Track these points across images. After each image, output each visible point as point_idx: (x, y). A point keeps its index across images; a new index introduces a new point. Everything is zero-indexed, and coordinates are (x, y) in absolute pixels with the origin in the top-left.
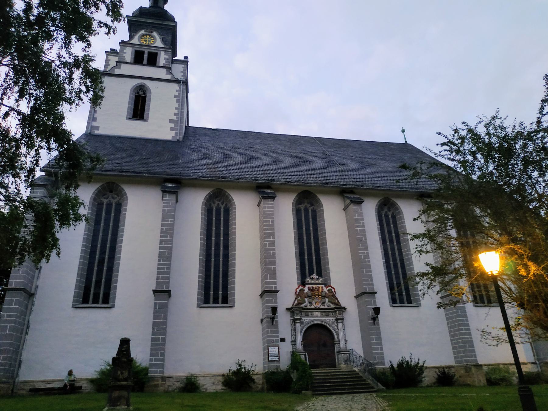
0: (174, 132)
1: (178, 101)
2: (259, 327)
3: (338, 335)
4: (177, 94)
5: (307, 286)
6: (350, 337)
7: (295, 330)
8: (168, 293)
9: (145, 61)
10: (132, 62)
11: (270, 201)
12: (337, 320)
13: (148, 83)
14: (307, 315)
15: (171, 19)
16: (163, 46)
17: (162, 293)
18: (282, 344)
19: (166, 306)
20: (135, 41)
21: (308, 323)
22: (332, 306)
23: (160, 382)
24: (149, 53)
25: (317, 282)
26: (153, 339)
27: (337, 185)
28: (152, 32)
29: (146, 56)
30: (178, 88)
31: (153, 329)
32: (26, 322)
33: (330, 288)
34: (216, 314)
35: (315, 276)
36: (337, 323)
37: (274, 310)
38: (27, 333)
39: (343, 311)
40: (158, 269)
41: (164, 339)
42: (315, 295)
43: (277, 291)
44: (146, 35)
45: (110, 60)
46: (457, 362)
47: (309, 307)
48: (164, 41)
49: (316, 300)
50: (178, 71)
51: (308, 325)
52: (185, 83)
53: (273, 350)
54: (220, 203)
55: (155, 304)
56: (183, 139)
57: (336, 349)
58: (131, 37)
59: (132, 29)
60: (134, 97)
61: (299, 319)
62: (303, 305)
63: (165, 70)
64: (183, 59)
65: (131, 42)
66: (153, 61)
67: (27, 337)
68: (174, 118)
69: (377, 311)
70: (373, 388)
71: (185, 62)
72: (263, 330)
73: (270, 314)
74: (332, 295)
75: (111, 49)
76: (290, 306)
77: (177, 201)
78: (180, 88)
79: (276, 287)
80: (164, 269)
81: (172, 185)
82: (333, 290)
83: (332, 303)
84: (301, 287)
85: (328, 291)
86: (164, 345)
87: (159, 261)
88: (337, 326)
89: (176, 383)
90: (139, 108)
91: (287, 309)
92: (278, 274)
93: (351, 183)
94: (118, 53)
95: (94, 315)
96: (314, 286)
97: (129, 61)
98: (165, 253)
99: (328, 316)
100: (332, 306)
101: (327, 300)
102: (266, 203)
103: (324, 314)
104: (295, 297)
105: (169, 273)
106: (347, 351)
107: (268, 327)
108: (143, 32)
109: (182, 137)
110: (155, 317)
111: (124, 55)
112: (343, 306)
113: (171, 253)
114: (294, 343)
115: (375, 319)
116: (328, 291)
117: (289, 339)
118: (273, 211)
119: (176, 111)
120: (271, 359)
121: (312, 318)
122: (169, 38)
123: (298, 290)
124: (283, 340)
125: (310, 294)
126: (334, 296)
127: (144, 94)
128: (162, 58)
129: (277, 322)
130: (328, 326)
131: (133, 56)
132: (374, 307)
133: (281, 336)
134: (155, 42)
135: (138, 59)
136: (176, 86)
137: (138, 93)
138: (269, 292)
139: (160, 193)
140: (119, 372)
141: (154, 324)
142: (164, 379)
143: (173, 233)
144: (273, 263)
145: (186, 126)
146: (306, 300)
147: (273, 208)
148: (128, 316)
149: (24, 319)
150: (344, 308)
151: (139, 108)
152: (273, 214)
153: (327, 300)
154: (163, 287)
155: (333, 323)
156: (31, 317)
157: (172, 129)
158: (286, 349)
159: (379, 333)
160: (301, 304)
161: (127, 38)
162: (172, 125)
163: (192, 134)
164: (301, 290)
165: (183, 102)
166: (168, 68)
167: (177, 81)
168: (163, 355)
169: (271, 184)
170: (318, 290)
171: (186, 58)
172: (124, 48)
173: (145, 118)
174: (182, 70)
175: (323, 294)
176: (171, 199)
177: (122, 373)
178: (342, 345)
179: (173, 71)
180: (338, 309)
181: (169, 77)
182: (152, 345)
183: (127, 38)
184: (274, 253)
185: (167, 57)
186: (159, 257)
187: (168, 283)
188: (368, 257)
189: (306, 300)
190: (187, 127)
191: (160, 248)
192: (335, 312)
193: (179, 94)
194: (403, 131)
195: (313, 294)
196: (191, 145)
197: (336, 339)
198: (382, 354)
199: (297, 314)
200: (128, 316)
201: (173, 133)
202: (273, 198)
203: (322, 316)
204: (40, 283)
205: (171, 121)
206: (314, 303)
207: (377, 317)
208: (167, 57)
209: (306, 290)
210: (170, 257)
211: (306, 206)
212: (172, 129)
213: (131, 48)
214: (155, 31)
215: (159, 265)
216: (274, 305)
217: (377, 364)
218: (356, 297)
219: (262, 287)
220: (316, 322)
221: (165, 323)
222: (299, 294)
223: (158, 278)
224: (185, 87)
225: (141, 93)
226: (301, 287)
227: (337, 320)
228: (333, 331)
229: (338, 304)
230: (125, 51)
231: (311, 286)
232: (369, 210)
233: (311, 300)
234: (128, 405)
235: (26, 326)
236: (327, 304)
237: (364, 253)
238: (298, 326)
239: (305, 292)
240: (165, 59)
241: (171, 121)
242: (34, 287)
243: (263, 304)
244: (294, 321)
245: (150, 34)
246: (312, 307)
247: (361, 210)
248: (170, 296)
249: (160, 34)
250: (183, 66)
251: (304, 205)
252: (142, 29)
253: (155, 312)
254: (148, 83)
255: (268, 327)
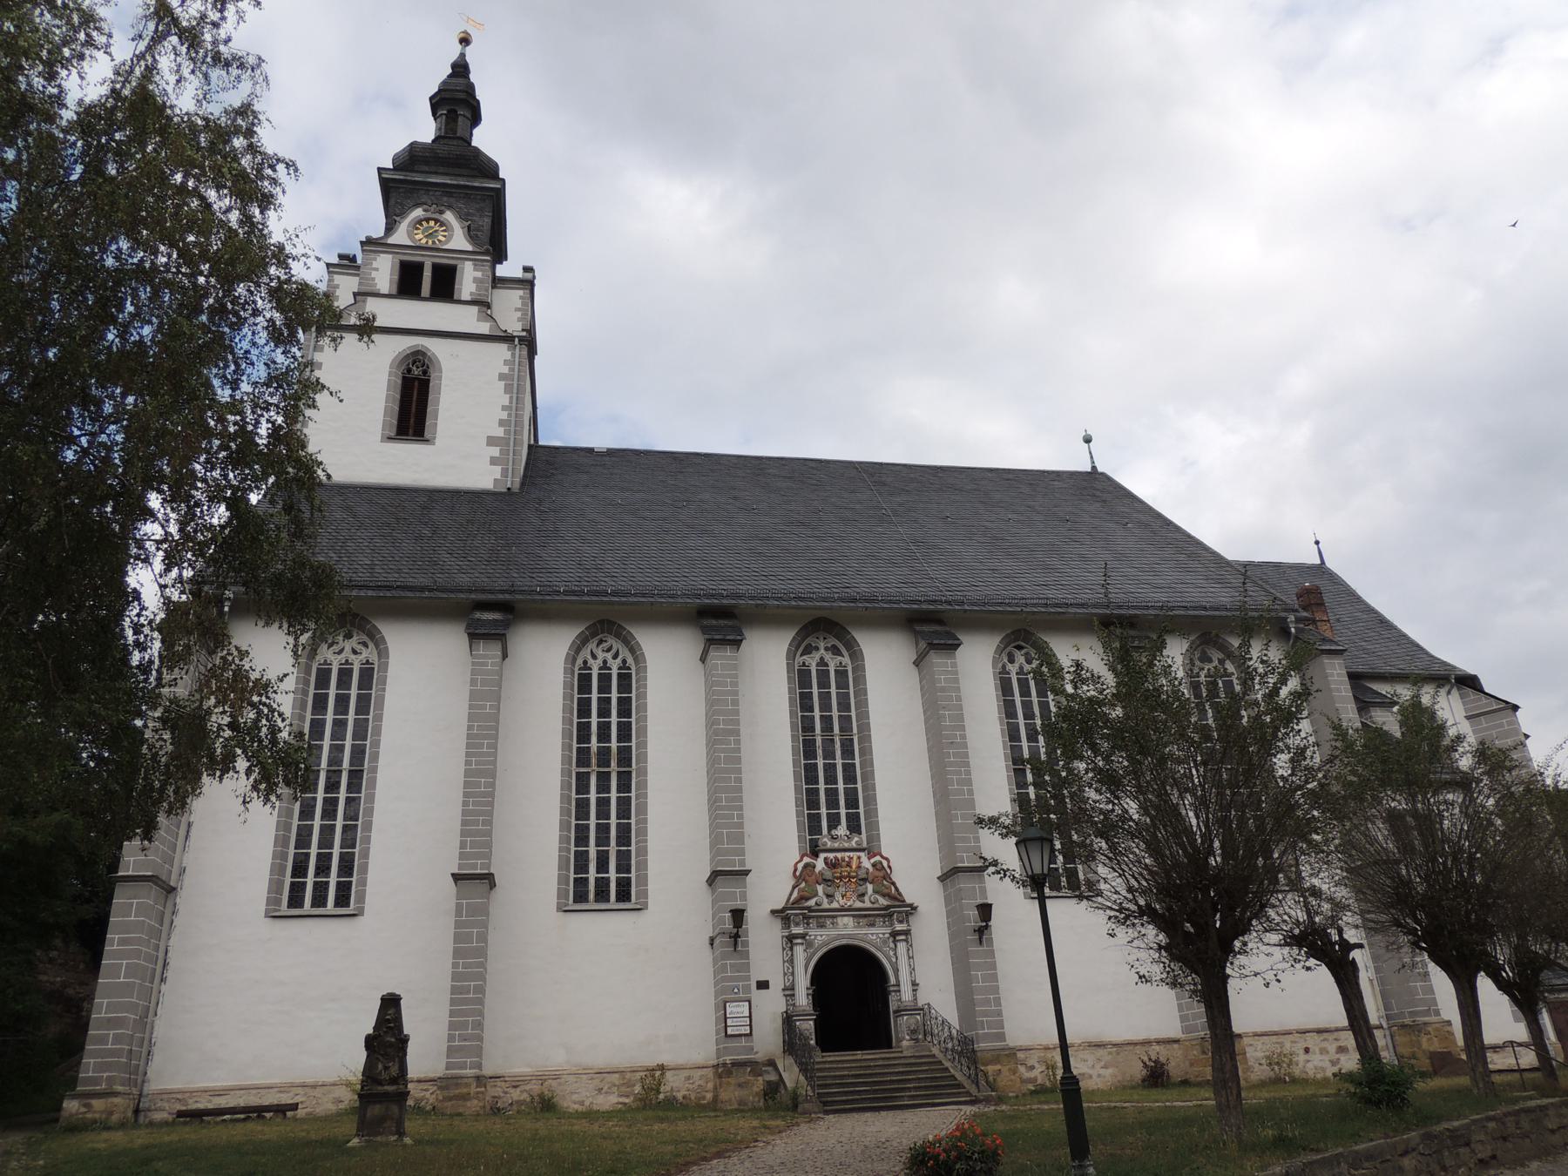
0: (498, 469)
1: (508, 389)
2: (706, 955)
3: (896, 971)
4: (506, 370)
5: (822, 856)
6: (925, 977)
7: (791, 961)
8: (488, 879)
9: (426, 288)
10: (394, 292)
11: (728, 652)
12: (894, 934)
13: (434, 346)
14: (822, 926)
15: (488, 169)
16: (469, 248)
17: (475, 881)
18: (756, 995)
19: (484, 911)
20: (400, 237)
21: (825, 944)
22: (883, 902)
23: (473, 1089)
24: (437, 268)
25: (846, 845)
26: (454, 990)
27: (898, 602)
28: (442, 212)
29: (427, 274)
30: (508, 355)
31: (455, 965)
32: (161, 955)
33: (878, 858)
34: (602, 928)
35: (842, 830)
36: (895, 942)
37: (738, 915)
38: (163, 980)
39: (908, 914)
40: (464, 823)
41: (481, 990)
42: (840, 878)
43: (746, 873)
44: (428, 220)
45: (337, 286)
46: (1186, 1030)
47: (826, 905)
48: (471, 234)
49: (842, 889)
50: (507, 305)
51: (825, 950)
52: (528, 342)
53: (737, 1010)
54: (609, 656)
55: (459, 908)
56: (523, 484)
57: (893, 1006)
58: (390, 228)
59: (392, 202)
60: (399, 382)
61: (803, 936)
62: (812, 903)
63: (475, 309)
64: (519, 274)
65: (390, 241)
66: (444, 287)
67: (163, 987)
68: (500, 432)
69: (985, 910)
70: (968, 1093)
71: (527, 283)
72: (715, 961)
73: (729, 925)
74: (882, 876)
75: (341, 257)
76: (780, 906)
77: (505, 656)
78: (513, 355)
79: (742, 862)
80: (476, 823)
81: (492, 616)
82: (885, 863)
83: (884, 895)
84: (807, 860)
85: (874, 865)
86: (481, 1002)
87: (465, 804)
88: (895, 949)
89: (511, 1090)
90: (412, 411)
91: (773, 912)
92: (747, 829)
93: (933, 595)
94: (358, 268)
95: (316, 936)
96: (839, 855)
97: (385, 289)
98: (478, 785)
99: (872, 925)
100: (883, 902)
101: (870, 887)
102: (719, 656)
103: (863, 921)
104: (792, 882)
105: (489, 833)
106: (915, 1009)
107: (724, 956)
108: (418, 213)
109: (518, 480)
110: (457, 938)
111: (374, 274)
112: (908, 901)
113: (493, 785)
114: (789, 991)
115: (982, 931)
116: (874, 865)
117: (777, 983)
118: (736, 676)
119: (504, 415)
120: (730, 1031)
121: (834, 932)
122: (486, 222)
123: (800, 866)
124: (763, 985)
125: (828, 874)
126: (887, 877)
127: (425, 372)
128: (469, 280)
129: (746, 944)
130: (873, 950)
131: (396, 277)
132: (980, 901)
133: (757, 975)
134: (449, 238)
135: (408, 283)
136: (501, 351)
137: (409, 371)
138: (726, 875)
139: (464, 640)
140: (380, 1066)
141: (457, 953)
142: (479, 1079)
143: (496, 737)
144: (736, 802)
145: (530, 446)
146: (820, 889)
147: (735, 667)
148: (392, 940)
149: (157, 948)
150: (911, 905)
151: (412, 411)
152: (735, 684)
153: (870, 887)
154: (474, 866)
155: (885, 942)
156: (171, 943)
157: (494, 461)
158: (771, 1006)
159: (993, 966)
160: (807, 899)
161: (378, 231)
162: (495, 451)
163: (547, 468)
164: (806, 866)
165: (520, 390)
166: (482, 304)
167: (507, 338)
168: (479, 1025)
169: (734, 606)
170: (849, 865)
171: (527, 269)
172: (372, 256)
173: (427, 435)
174: (519, 304)
175: (862, 874)
176: (490, 651)
177: (386, 1068)
178: (906, 995)
179: (497, 310)
180: (897, 910)
181: (484, 328)
182: (453, 1002)
183: (378, 231)
184: (739, 780)
185: (479, 274)
186: (466, 795)
187: (488, 856)
188: (969, 782)
189: (820, 889)
190: (534, 449)
191: (467, 773)
192: (891, 915)
193: (512, 370)
194: (1088, 440)
195: (838, 873)
196: (540, 502)
197: (893, 980)
198: (1000, 1014)
199: (797, 924)
200: (392, 940)
201: (497, 471)
202: (737, 643)
203: (858, 926)
204: (189, 860)
205: (491, 441)
206: (838, 896)
207: (987, 927)
208: (479, 274)
209: (820, 864)
210: (492, 795)
211: (822, 659)
212: (494, 461)
213: (390, 256)
214: (450, 207)
215: (464, 813)
216: (738, 904)
217: (987, 1037)
218: (942, 878)
219: (712, 860)
220: (844, 942)
221: (482, 952)
222: (804, 876)
223: (463, 845)
224: (525, 352)
225: (416, 372)
226: (807, 860)
227: (894, 934)
228: (885, 961)
229: (897, 898)
230: (375, 265)
231: (831, 856)
232: (977, 663)
233: (830, 890)
234: (401, 1133)
235: (160, 963)
236: (872, 898)
237: (959, 773)
238: (800, 952)
239: (818, 869)
240: (475, 280)
241: (491, 441)
242: (175, 871)
243: (714, 902)
244: (791, 939)
245: (436, 216)
246: (835, 905)
247: (954, 665)
248: (493, 885)
249: (462, 217)
250: (521, 292)
251: (816, 656)
252: (417, 205)
253: (458, 925)
254: (434, 346)
255: (724, 956)
